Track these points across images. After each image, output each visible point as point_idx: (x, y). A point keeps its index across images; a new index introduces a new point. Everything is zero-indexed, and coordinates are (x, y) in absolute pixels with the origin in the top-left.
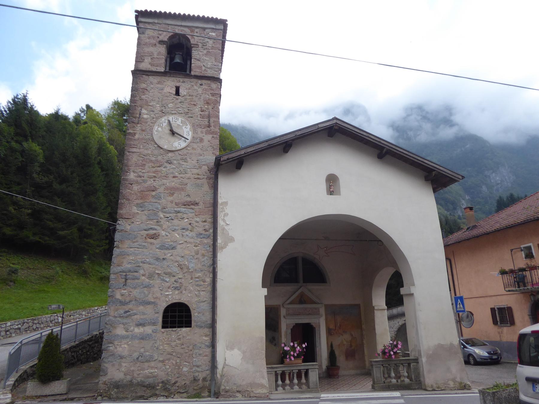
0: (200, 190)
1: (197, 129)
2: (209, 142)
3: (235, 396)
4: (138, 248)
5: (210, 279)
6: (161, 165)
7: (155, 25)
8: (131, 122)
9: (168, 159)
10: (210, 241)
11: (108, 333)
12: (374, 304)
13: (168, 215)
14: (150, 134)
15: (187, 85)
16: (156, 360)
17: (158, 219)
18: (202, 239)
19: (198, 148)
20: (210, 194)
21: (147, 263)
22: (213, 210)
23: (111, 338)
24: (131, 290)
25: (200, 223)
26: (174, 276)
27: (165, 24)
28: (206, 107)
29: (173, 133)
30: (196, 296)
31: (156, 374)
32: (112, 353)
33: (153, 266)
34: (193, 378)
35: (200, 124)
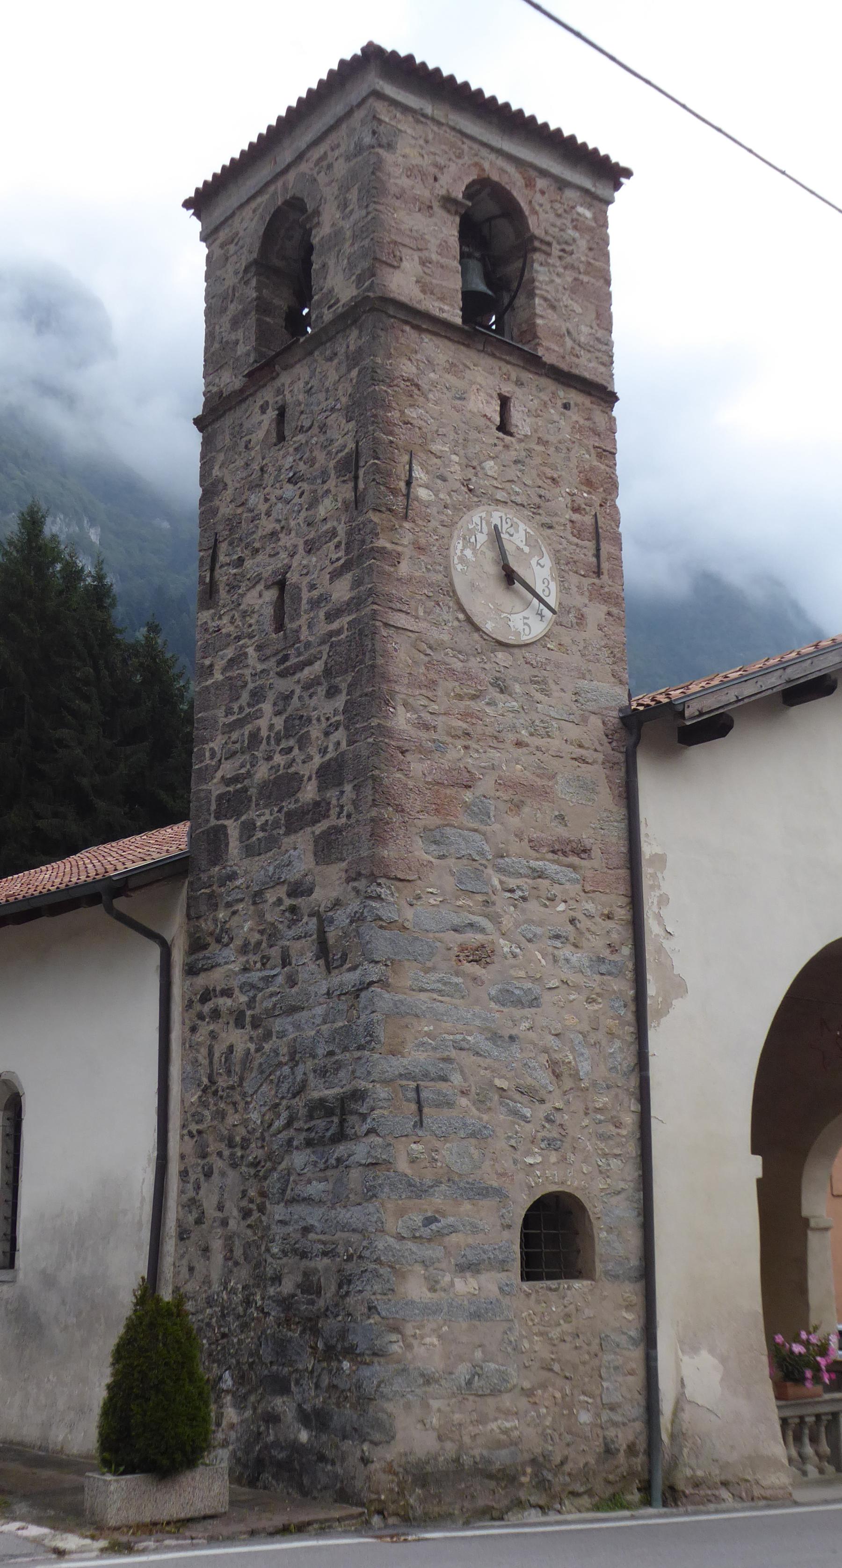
0: (590, 804)
1: (566, 575)
2: (601, 629)
3: (718, 1499)
4: (440, 992)
5: (631, 1115)
6: (478, 693)
7: (422, 122)
8: (384, 509)
9: (498, 675)
10: (624, 987)
11: (385, 1294)
12: (806, 1211)
13: (512, 883)
14: (441, 568)
15: (531, 398)
16: (515, 1386)
17: (486, 893)
18: (605, 977)
19: (574, 648)
20: (617, 822)
21: (468, 1049)
22: (628, 878)
23: (397, 1312)
24: (438, 1144)
25: (598, 919)
26: (542, 1101)
27: (453, 129)
28: (584, 498)
29: (509, 577)
30: (600, 1172)
31: (516, 1433)
32: (400, 1367)
33: (488, 1061)
34: (603, 1445)
35: (576, 558)
